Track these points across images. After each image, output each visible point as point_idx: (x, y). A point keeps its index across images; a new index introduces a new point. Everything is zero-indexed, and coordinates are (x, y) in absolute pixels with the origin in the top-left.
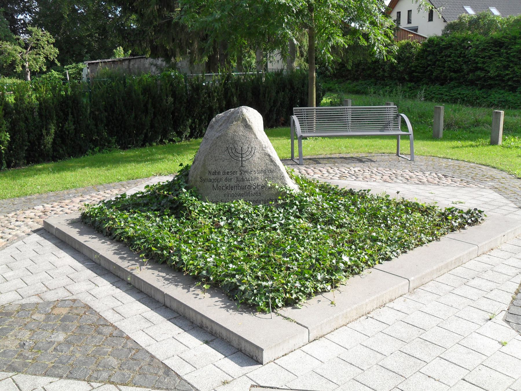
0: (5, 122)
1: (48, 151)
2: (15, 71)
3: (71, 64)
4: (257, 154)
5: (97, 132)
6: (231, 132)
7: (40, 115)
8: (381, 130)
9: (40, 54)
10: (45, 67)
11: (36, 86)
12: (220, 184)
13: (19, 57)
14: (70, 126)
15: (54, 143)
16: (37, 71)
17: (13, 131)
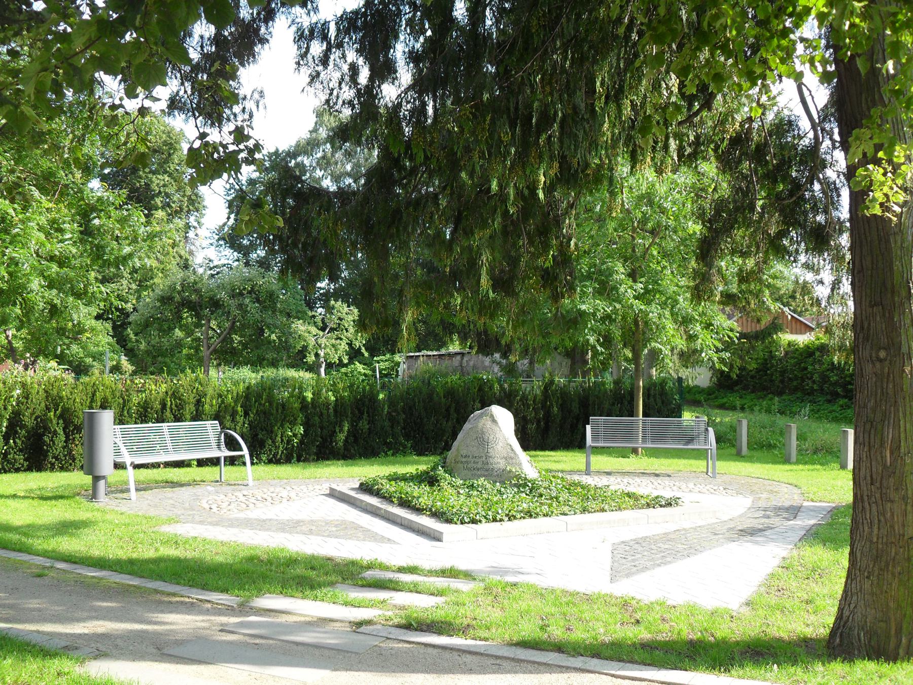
0: (301, 415)
1: (339, 449)
2: (305, 360)
3: (384, 355)
4: (501, 444)
5: (393, 435)
6: (480, 425)
7: (335, 411)
8: (684, 445)
9: (341, 339)
10: (347, 357)
11: (334, 382)
12: (469, 466)
13: (312, 341)
14: (364, 425)
15: (346, 441)
16: (335, 362)
17: (307, 425)
